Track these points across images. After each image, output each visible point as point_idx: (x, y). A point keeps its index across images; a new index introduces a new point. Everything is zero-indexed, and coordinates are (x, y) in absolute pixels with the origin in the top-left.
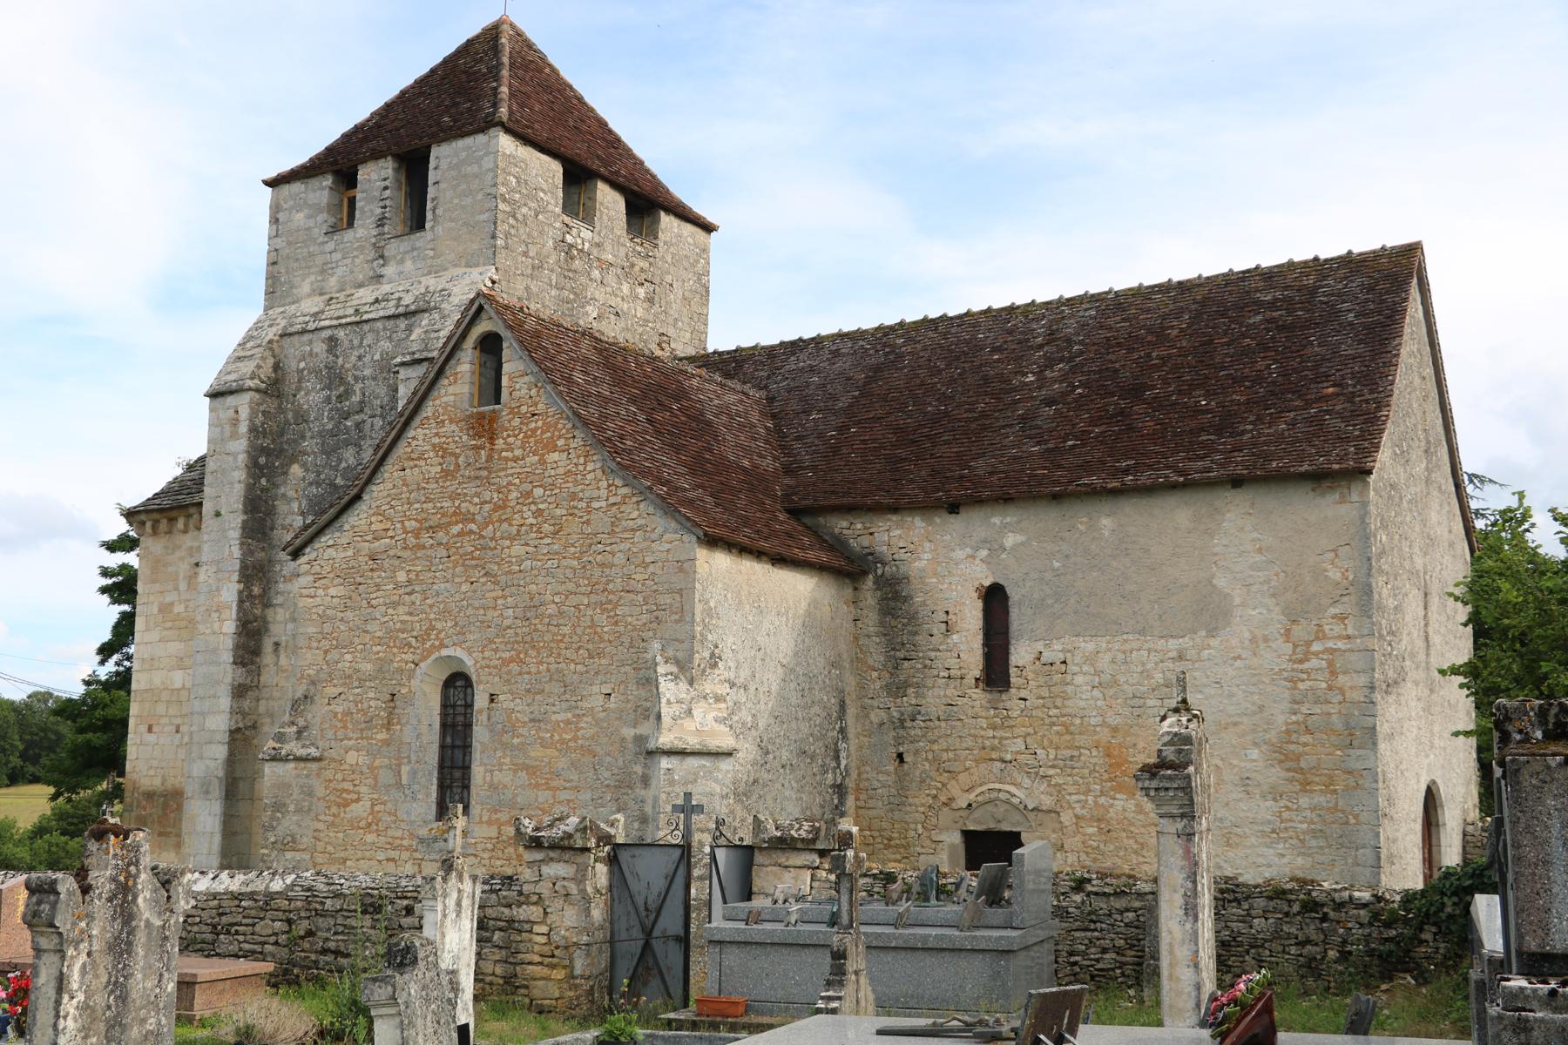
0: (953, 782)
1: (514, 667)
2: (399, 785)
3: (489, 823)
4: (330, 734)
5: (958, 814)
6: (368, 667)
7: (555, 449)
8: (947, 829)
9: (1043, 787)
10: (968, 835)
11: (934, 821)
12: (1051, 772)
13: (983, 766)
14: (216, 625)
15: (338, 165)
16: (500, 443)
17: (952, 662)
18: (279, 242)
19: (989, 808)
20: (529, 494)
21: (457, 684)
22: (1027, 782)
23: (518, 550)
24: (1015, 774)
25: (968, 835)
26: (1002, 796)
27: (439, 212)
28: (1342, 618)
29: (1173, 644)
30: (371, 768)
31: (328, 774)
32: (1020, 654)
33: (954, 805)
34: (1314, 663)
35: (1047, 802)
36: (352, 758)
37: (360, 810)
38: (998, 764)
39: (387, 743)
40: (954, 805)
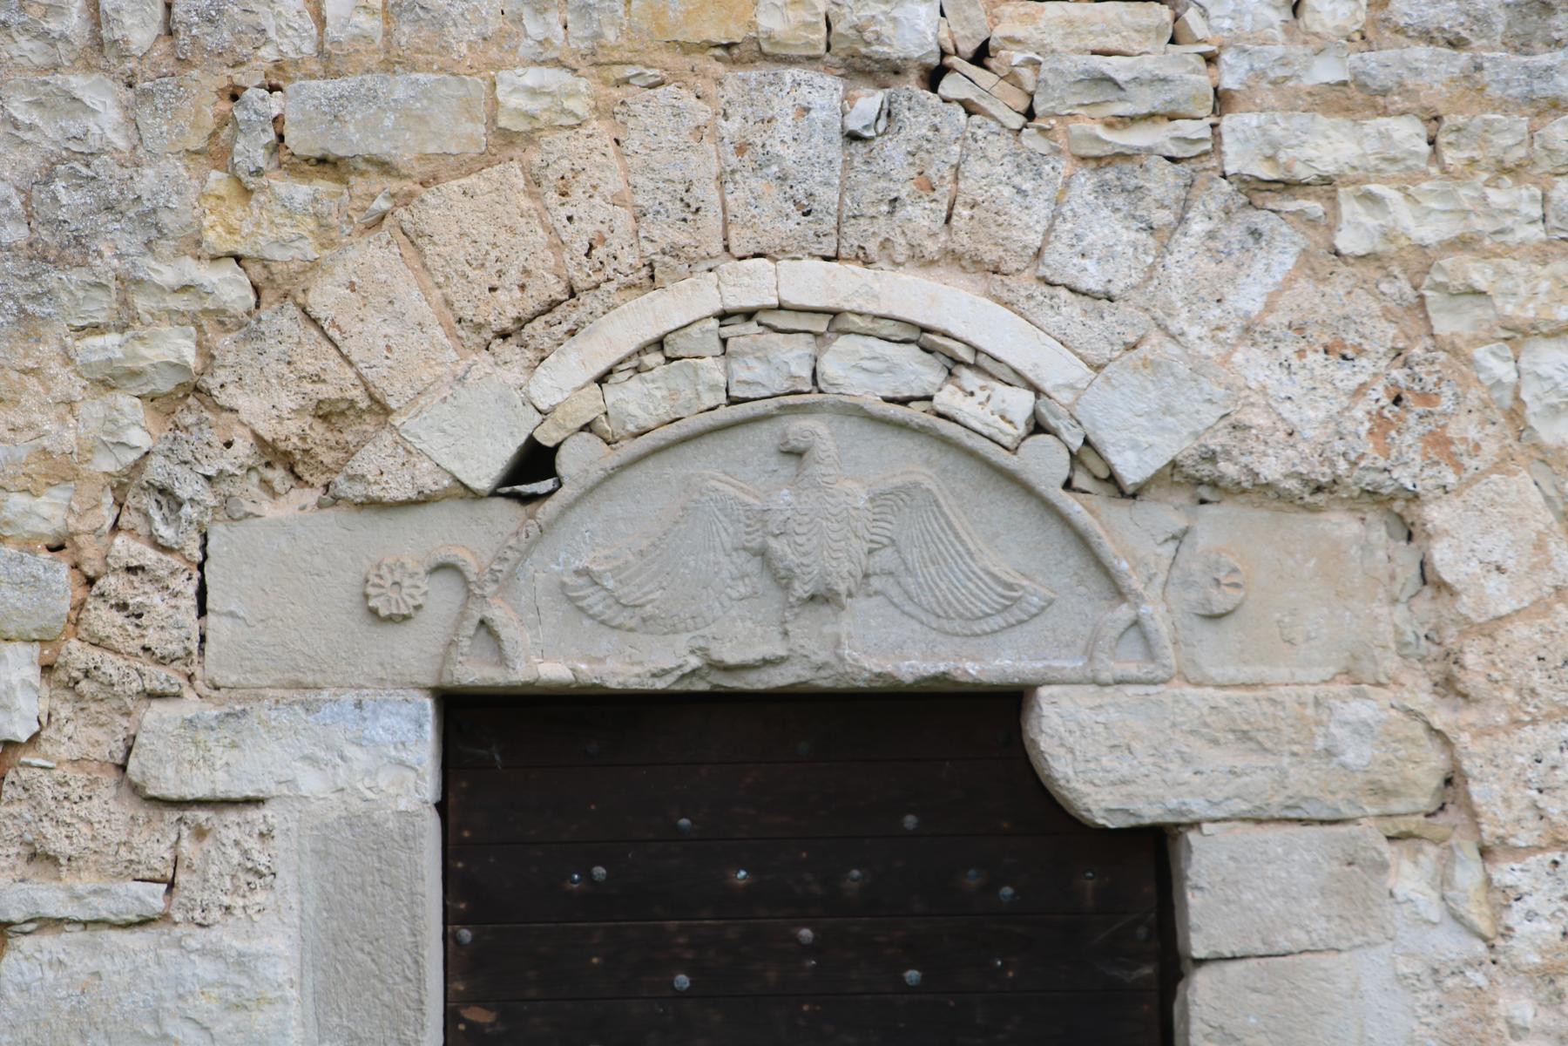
0: (375, 256)
5: (411, 543)
8: (303, 689)
9: (1267, 274)
10: (480, 728)
11: (169, 614)
12: (1329, 146)
13: (659, 117)
19: (737, 476)
22: (1101, 242)
24: (990, 171)
25: (480, 728)
26: (856, 369)
33: (379, 466)
35: (1304, 410)
38: (823, 92)
40: (379, 466)
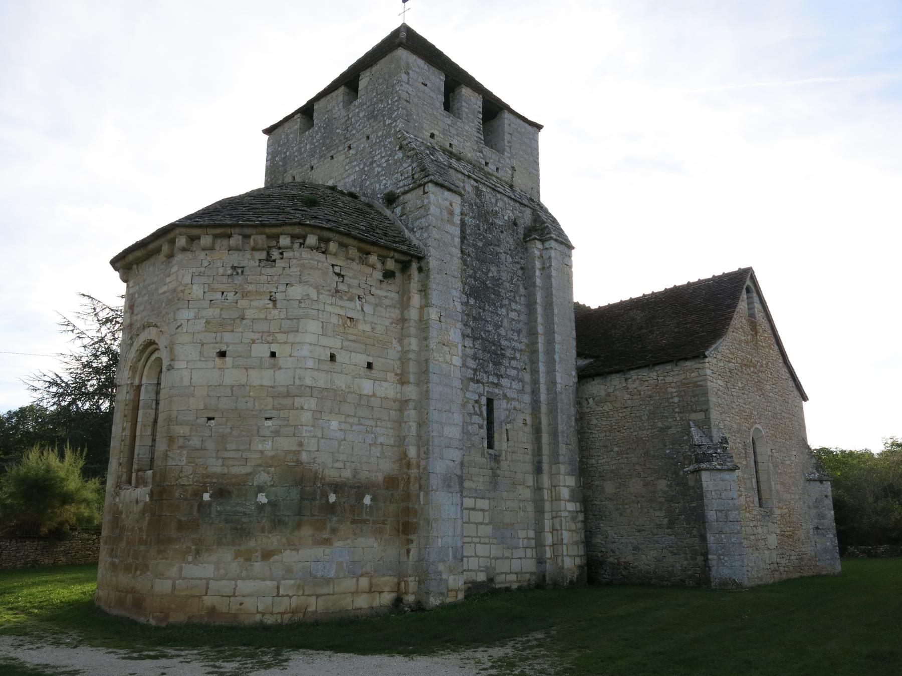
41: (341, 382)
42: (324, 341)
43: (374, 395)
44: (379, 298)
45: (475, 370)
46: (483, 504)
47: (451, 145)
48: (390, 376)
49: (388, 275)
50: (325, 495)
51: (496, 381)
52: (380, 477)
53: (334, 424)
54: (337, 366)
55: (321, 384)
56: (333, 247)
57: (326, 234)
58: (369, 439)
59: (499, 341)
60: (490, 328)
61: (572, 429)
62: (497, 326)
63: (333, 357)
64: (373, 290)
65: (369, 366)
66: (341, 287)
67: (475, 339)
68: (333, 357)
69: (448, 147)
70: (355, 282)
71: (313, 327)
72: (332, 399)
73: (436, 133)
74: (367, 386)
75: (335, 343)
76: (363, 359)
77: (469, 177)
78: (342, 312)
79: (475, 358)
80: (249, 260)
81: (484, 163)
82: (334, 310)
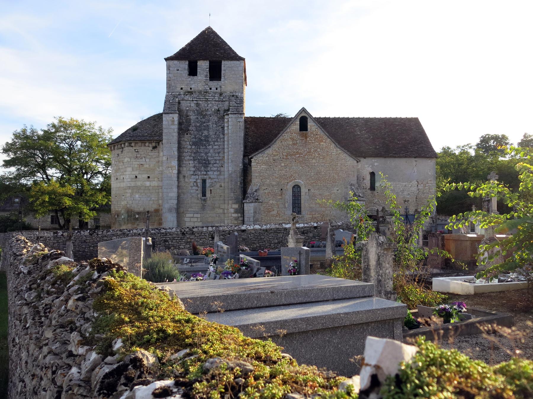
1: (314, 184)
2: (285, 207)
3: (310, 214)
4: (264, 197)
6: (274, 183)
7: (323, 142)
14: (171, 171)
15: (180, 56)
16: (308, 139)
17: (364, 185)
18: (171, 75)
20: (316, 150)
21: (297, 189)
23: (314, 161)
27: (226, 77)
28: (431, 181)
29: (404, 184)
30: (277, 204)
31: (265, 205)
32: (377, 184)
34: (427, 188)
36: (271, 202)
37: (275, 213)
39: (281, 199)
41: (139, 184)
42: (133, 173)
43: (150, 186)
44: (151, 156)
45: (194, 171)
46: (199, 215)
47: (191, 89)
48: (156, 179)
49: (154, 148)
50: (135, 215)
51: (205, 173)
52: (153, 210)
53: (137, 196)
54: (137, 179)
55: (133, 185)
56: (133, 144)
57: (129, 142)
58: (149, 199)
59: (207, 158)
60: (203, 154)
61: (238, 187)
62: (206, 153)
63: (136, 177)
64: (149, 154)
65: (149, 177)
66: (138, 155)
67: (194, 160)
68: (136, 177)
69: (189, 90)
70: (143, 153)
71: (129, 169)
72: (135, 189)
73: (183, 87)
74: (148, 184)
75: (136, 173)
76: (146, 176)
77: (193, 100)
78: (138, 163)
79: (194, 167)
80: (119, 151)
81: (209, 89)
82: (136, 163)
